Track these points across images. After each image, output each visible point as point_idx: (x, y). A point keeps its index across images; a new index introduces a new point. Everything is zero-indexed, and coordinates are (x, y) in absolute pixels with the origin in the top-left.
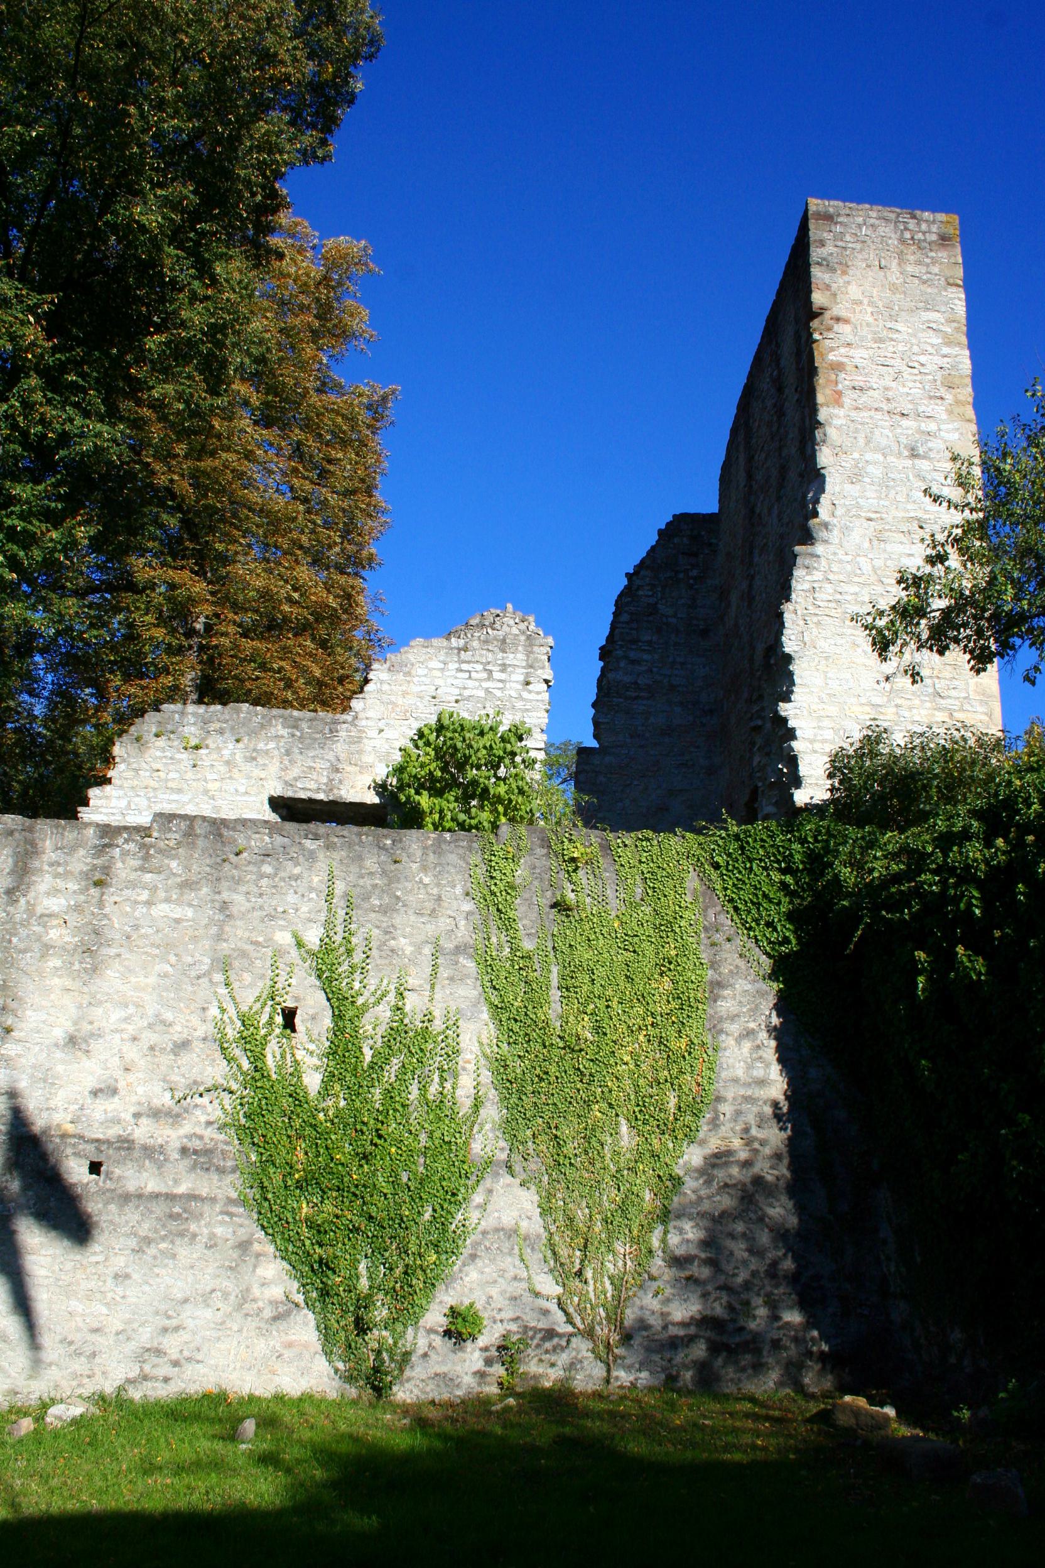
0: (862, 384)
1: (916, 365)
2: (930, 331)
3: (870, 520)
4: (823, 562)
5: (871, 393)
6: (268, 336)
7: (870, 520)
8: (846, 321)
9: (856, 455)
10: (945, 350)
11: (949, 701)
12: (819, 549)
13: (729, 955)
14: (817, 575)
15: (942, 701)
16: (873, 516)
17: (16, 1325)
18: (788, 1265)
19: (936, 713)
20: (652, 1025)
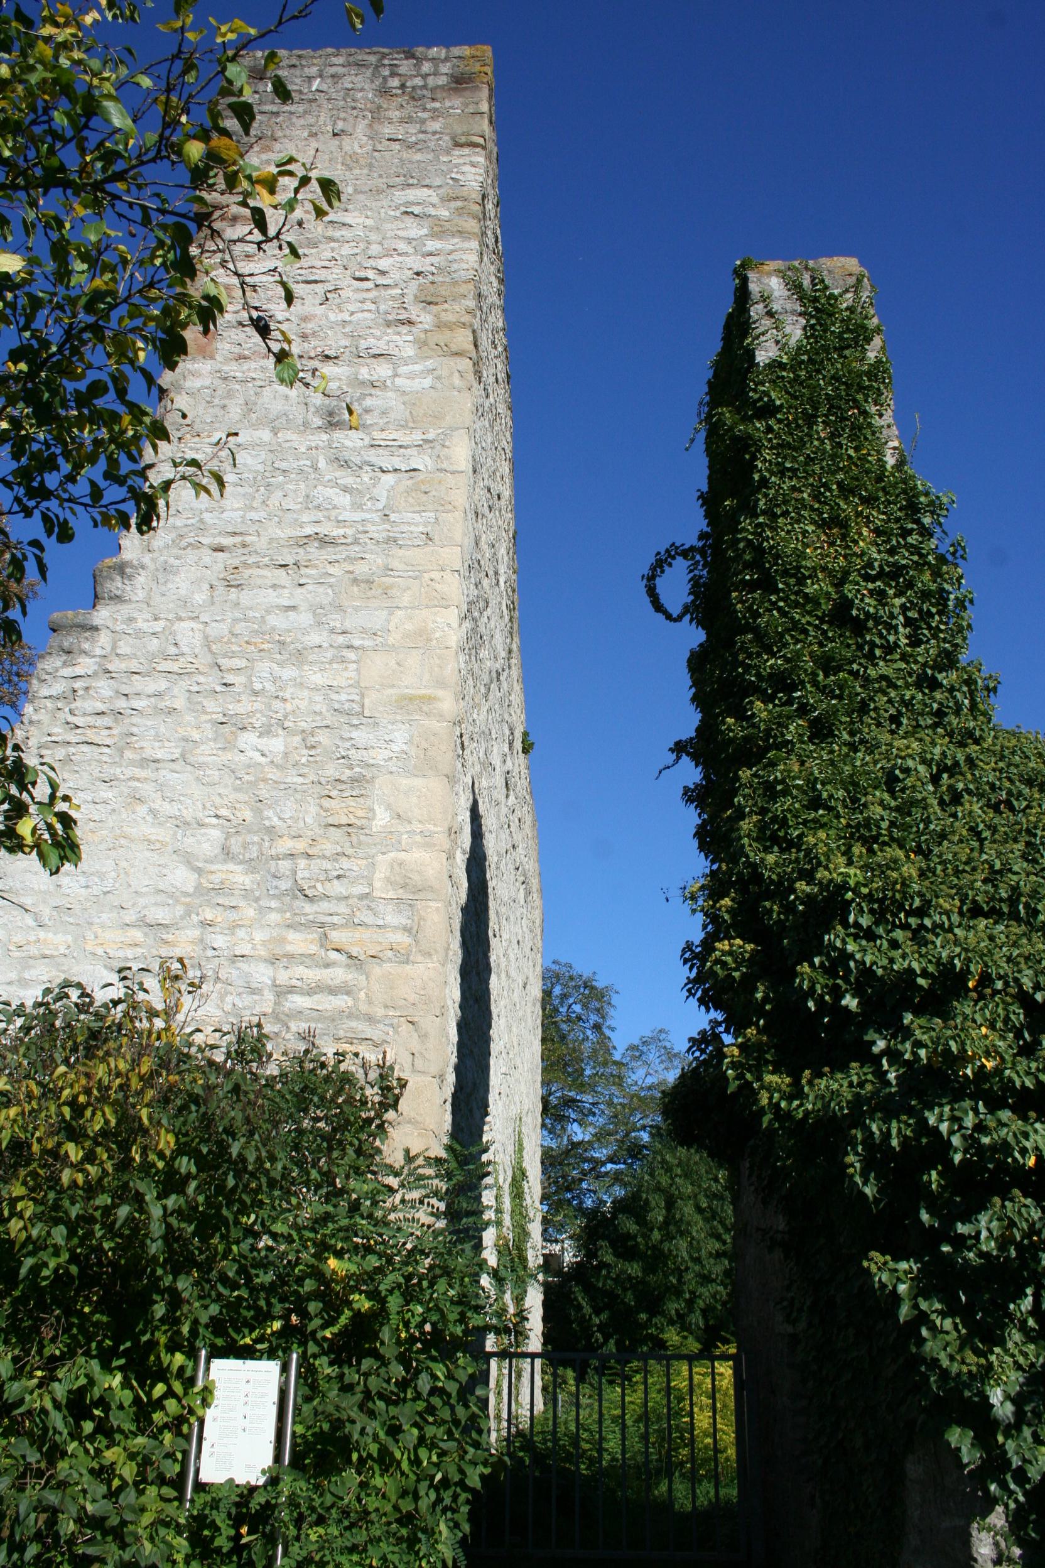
1: (370, 274)
3: (220, 549)
4: (104, 638)
7: (220, 549)
10: (432, 245)
11: (325, 906)
15: (308, 908)
16: (227, 541)
19: (292, 936)
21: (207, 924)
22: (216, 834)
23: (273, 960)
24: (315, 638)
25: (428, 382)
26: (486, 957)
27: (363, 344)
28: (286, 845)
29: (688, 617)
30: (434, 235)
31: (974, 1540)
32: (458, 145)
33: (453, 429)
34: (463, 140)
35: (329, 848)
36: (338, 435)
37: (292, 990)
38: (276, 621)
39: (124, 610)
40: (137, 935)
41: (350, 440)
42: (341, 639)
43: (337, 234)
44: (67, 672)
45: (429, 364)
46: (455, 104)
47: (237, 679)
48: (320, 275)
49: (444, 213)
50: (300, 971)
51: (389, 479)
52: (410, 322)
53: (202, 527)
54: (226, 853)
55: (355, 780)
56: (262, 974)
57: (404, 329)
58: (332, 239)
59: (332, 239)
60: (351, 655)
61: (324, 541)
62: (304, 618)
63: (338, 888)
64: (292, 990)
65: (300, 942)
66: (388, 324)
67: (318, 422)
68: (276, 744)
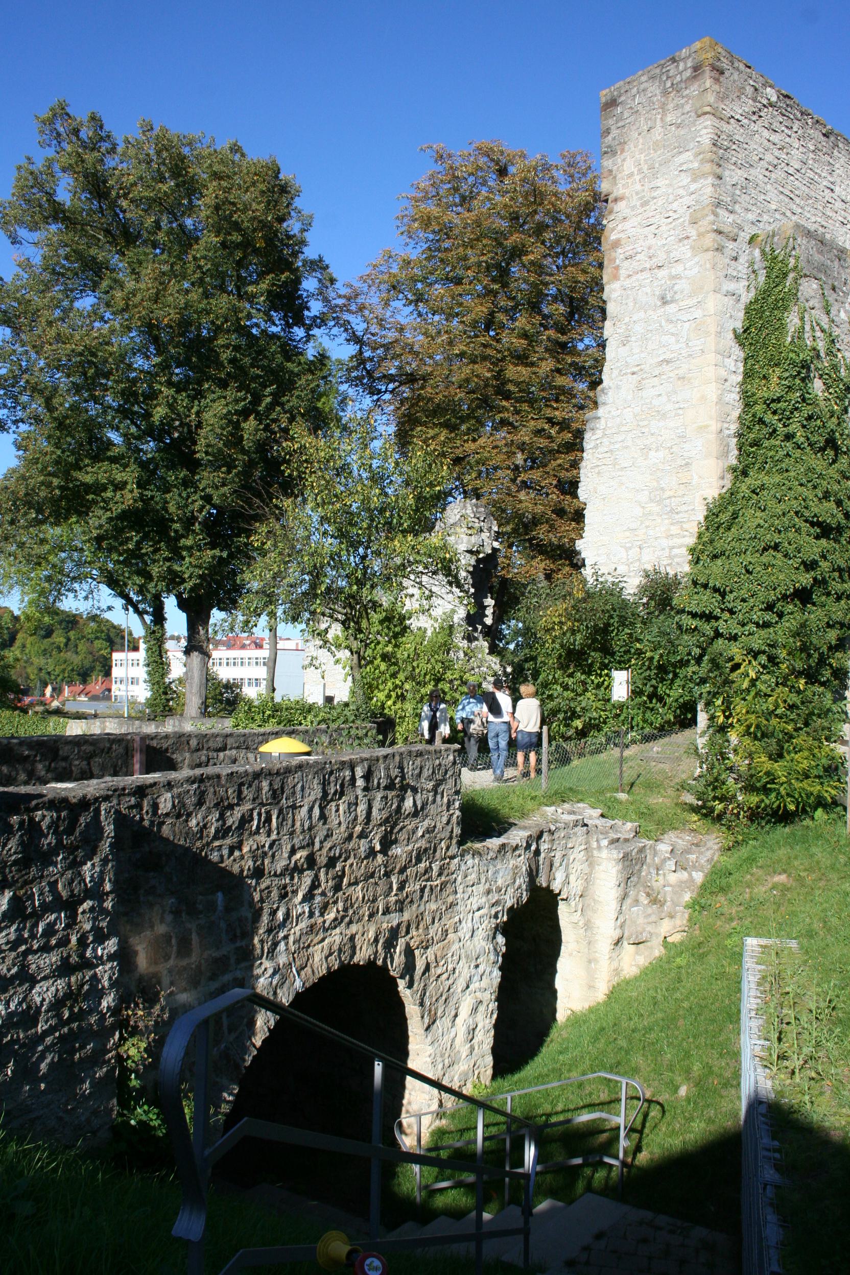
0: (630, 253)
1: (671, 214)
2: (683, 174)
3: (633, 374)
4: (603, 421)
5: (638, 257)
6: (199, 145)
7: (633, 374)
8: (622, 199)
9: (627, 319)
10: (693, 187)
11: (681, 515)
12: (601, 411)
13: (147, 284)
14: (599, 433)
15: (677, 517)
16: (635, 369)
17: (724, 418)
18: (472, 590)
19: (672, 528)
20: (465, 258)
21: (647, 527)
22: (646, 493)
23: (667, 537)
24: (670, 407)
25: (696, 270)
26: (496, 1037)
27: (672, 255)
28: (668, 494)
29: (450, 1101)
30: (694, 180)
31: (797, 1119)
32: (699, 116)
33: (708, 293)
34: (700, 112)
35: (680, 493)
36: (667, 307)
37: (673, 547)
38: (656, 402)
39: (607, 408)
40: (627, 534)
41: (671, 308)
42: (677, 406)
43: (655, 194)
44: (594, 438)
45: (696, 259)
46: (694, 89)
47: (645, 430)
48: (652, 220)
49: (696, 165)
50: (675, 540)
51: (687, 325)
52: (688, 237)
53: (627, 365)
54: (651, 500)
55: (687, 464)
56: (665, 543)
57: (686, 242)
58: (654, 198)
59: (654, 198)
60: (681, 412)
61: (668, 362)
62: (664, 399)
63: (684, 508)
64: (673, 547)
65: (675, 530)
66: (680, 240)
67: (659, 303)
68: (661, 454)
